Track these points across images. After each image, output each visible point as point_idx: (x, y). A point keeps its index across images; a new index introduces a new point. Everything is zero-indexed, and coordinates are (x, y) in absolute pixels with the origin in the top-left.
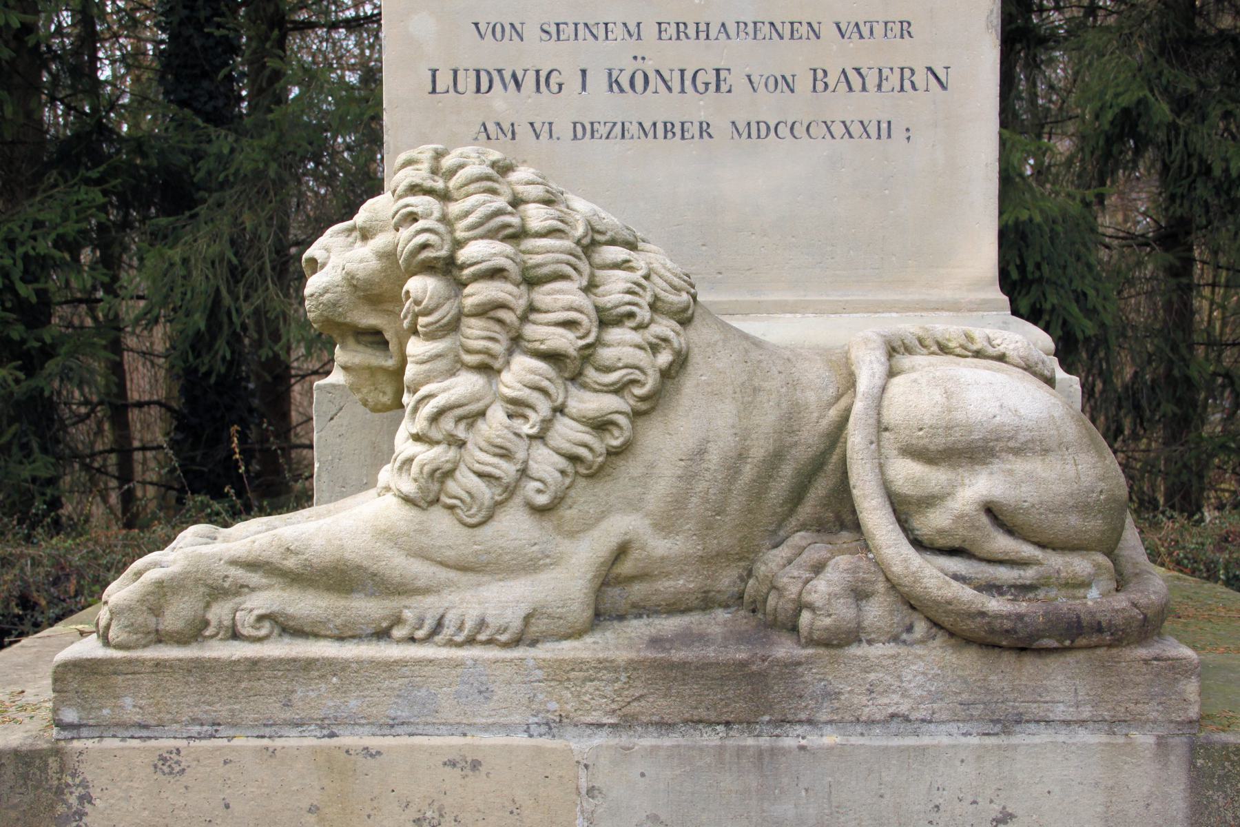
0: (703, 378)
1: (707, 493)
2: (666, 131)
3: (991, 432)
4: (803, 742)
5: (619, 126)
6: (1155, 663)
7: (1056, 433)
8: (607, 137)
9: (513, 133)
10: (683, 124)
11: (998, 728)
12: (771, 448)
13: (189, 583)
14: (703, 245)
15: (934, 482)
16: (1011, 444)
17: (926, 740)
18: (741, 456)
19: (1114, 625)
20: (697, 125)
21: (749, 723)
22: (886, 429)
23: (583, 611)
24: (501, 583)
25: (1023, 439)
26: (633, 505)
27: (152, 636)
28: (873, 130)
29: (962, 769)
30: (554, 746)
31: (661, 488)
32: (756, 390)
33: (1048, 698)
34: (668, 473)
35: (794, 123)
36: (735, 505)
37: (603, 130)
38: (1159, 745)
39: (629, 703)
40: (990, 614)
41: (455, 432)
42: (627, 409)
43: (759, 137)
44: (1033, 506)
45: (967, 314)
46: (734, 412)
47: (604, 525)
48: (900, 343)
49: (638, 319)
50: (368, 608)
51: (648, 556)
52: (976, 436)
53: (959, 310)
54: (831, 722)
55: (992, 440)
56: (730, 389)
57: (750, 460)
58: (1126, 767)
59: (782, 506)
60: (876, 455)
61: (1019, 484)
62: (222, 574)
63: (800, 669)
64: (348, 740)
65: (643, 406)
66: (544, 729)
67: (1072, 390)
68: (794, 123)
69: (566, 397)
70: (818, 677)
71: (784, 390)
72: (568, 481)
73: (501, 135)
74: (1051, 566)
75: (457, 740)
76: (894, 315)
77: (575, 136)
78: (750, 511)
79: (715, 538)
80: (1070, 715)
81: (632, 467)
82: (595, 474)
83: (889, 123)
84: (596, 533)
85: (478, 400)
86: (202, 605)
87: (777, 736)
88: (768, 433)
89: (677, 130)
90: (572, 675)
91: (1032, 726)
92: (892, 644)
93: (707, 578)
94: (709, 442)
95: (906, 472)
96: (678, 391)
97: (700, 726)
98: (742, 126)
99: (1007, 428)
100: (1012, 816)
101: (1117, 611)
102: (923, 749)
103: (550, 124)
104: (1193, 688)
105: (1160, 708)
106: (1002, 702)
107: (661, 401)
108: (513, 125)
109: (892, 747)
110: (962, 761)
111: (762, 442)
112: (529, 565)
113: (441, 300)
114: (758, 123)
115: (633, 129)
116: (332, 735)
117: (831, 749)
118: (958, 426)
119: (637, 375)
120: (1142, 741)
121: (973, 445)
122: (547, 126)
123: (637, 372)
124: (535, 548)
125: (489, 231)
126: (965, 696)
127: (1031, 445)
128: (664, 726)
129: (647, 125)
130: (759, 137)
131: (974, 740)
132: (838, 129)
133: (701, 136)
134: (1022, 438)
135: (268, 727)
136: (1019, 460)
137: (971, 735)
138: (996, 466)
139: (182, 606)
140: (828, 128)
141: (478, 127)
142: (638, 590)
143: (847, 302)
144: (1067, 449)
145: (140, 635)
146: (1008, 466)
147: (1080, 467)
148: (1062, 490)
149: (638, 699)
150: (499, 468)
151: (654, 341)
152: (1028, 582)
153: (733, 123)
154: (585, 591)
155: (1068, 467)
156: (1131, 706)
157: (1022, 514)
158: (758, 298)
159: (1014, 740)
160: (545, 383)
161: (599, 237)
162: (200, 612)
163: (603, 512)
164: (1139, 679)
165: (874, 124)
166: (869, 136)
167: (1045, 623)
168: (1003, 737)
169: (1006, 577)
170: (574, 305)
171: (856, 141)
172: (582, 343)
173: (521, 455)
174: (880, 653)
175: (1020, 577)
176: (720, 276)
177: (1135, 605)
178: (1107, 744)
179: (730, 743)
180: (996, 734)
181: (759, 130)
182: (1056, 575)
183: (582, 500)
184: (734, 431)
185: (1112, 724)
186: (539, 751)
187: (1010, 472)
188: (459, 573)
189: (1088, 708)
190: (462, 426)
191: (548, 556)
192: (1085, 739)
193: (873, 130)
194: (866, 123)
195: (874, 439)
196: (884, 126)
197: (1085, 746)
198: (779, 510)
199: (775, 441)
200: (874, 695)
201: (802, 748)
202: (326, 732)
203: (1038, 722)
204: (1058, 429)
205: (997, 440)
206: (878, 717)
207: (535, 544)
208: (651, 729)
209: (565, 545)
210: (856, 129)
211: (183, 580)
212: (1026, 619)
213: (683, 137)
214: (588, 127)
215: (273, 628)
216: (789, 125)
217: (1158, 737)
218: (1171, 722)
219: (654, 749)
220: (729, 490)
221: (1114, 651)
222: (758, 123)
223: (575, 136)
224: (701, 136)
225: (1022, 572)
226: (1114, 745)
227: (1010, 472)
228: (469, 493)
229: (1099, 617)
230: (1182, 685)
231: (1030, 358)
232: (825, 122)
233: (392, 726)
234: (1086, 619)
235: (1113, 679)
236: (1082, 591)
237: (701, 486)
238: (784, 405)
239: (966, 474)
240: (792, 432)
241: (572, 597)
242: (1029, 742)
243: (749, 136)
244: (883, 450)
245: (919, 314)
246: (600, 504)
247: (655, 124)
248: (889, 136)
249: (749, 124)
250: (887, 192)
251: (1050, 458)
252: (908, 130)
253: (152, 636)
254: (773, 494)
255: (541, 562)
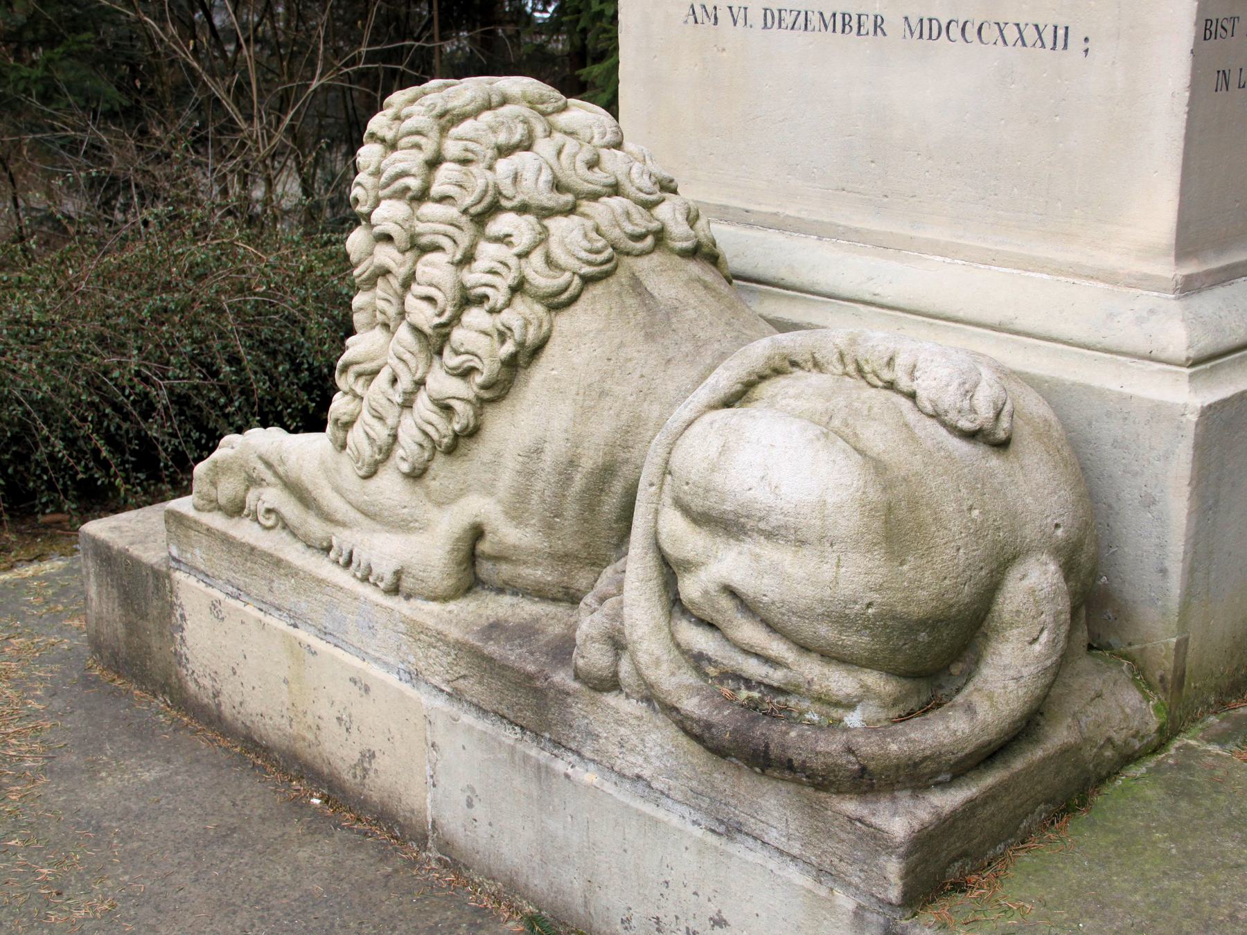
0: (554, 372)
1: (543, 493)
2: (844, 25)
3: (742, 505)
4: (570, 771)
5: (803, 14)
6: (859, 824)
7: (818, 523)
8: (793, 28)
9: (716, 18)
10: (859, 17)
11: (722, 829)
12: (600, 461)
13: (235, 467)
14: (872, 162)
15: (690, 546)
16: (762, 525)
17: (660, 814)
18: (572, 463)
19: (810, 768)
20: (872, 18)
21: (537, 734)
22: (670, 473)
23: (443, 579)
24: (388, 535)
25: (775, 523)
26: (488, 489)
27: (214, 504)
28: (1048, 36)
29: (686, 855)
30: (411, 695)
31: (507, 478)
32: (603, 394)
33: (763, 819)
34: (511, 465)
35: (966, 22)
36: (571, 509)
37: (788, 19)
38: (856, 914)
39: (458, 678)
40: (682, 712)
41: (353, 387)
42: (471, 396)
43: (930, 37)
44: (773, 603)
45: (1125, 290)
46: (571, 415)
47: (463, 502)
48: (808, 356)
49: (491, 302)
50: (316, 527)
51: (500, 542)
52: (728, 507)
53: (1116, 283)
54: (593, 761)
55: (742, 516)
56: (574, 389)
57: (580, 469)
58: (825, 923)
59: (616, 522)
60: (655, 499)
61: (761, 574)
62: (253, 465)
63: (569, 700)
64: (303, 635)
65: (486, 395)
66: (407, 677)
67: (1184, 419)
68: (966, 22)
69: (426, 373)
70: (582, 713)
71: (630, 399)
72: (426, 455)
73: (706, 19)
74: (802, 674)
75: (357, 662)
76: (1045, 276)
77: (766, 24)
78: (586, 521)
79: (559, 539)
80: (782, 843)
81: (482, 450)
82: (451, 450)
83: (1067, 28)
84: (455, 508)
85: (373, 360)
86: (243, 487)
87: (556, 756)
88: (599, 445)
89: (854, 23)
90: (422, 637)
91: (750, 841)
92: (645, 704)
93: (563, 574)
94: (545, 442)
95: (675, 528)
96: (526, 383)
97: (505, 721)
98: (914, 23)
99: (758, 506)
100: (726, 923)
101: (817, 754)
102: (656, 822)
103: (746, 8)
104: (893, 868)
105: (862, 875)
106: (725, 804)
107: (512, 390)
108: (715, 8)
109: (632, 808)
110: (687, 849)
111: (592, 453)
112: (403, 525)
113: (363, 256)
114: (930, 20)
115: (815, 19)
116: (295, 626)
117: (588, 787)
118: (714, 490)
119: (476, 363)
120: (842, 903)
121: (725, 516)
122: (742, 10)
123: (476, 359)
124: (405, 511)
125: (395, 192)
126: (694, 784)
127: (783, 532)
128: (482, 711)
129: (827, 16)
130: (930, 37)
131: (698, 832)
132: (1011, 34)
133: (875, 32)
134: (775, 520)
135: (267, 606)
136: (770, 546)
137: (699, 825)
138: (748, 546)
139: (227, 485)
140: (1001, 31)
141: (688, 10)
142: (506, 570)
143: (998, 252)
144: (832, 545)
145: (205, 502)
146: (758, 550)
147: (843, 570)
148: (809, 593)
149: (464, 677)
150: (374, 430)
151: (502, 328)
152: (775, 684)
153: (906, 18)
154: (443, 561)
155: (825, 567)
156: (836, 861)
157: (763, 608)
158: (913, 234)
159: (732, 848)
160: (407, 356)
161: (504, 203)
162: (241, 493)
163: (461, 489)
164: (843, 836)
165: (1050, 29)
166: (1043, 46)
167: (730, 742)
168: (724, 839)
169: (751, 671)
170: (434, 282)
171: (1029, 49)
172: (437, 321)
173: (391, 421)
174: (629, 710)
175: (767, 676)
176: (886, 200)
177: (850, 751)
178: (810, 891)
179: (519, 746)
180: (719, 834)
181: (931, 29)
182: (806, 686)
183: (443, 474)
184: (566, 435)
185: (821, 873)
186: (401, 693)
187: (757, 558)
188: (363, 517)
189: (798, 845)
190: (361, 381)
191: (417, 521)
192: (791, 876)
193: (1048, 36)
194: (1041, 28)
195: (655, 480)
196: (1061, 32)
197: (789, 883)
198: (614, 526)
199: (605, 454)
200: (624, 750)
201: (567, 776)
202: (292, 622)
203: (755, 838)
204: (823, 518)
205: (747, 517)
206: (627, 772)
207: (405, 507)
208: (473, 709)
209: (433, 513)
210: (1030, 35)
211: (232, 463)
212: (713, 730)
213: (859, 33)
214: (776, 15)
215: (277, 521)
216: (961, 26)
217: (860, 907)
218: (872, 895)
219: (470, 729)
220: (564, 495)
221: (822, 795)
222: (930, 20)
223: (766, 24)
224: (875, 32)
225: (771, 671)
226: (815, 895)
227: (757, 558)
228: (357, 450)
229: (791, 753)
230: (882, 860)
231: (939, 403)
232: (998, 24)
233: (325, 633)
234: (774, 751)
235: (820, 825)
236: (841, 711)
237: (539, 485)
238: (624, 417)
239: (721, 546)
240: (626, 448)
241: (432, 564)
242: (742, 856)
243: (921, 36)
244: (663, 496)
245: (1071, 280)
246: (458, 482)
247: (834, 15)
248: (1066, 45)
249: (921, 20)
250: (1058, 118)
251: (806, 551)
252: (1086, 39)
253: (214, 504)
254: (606, 508)
255: (412, 525)
